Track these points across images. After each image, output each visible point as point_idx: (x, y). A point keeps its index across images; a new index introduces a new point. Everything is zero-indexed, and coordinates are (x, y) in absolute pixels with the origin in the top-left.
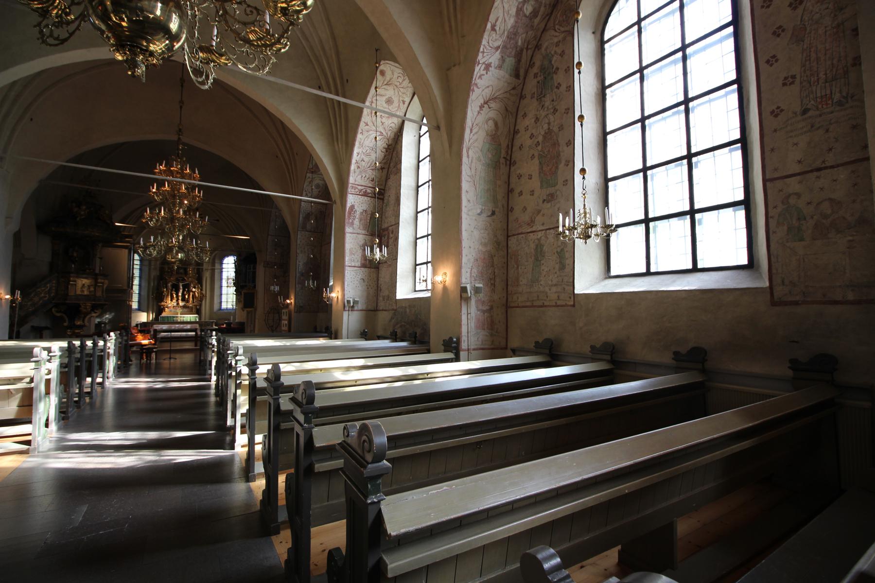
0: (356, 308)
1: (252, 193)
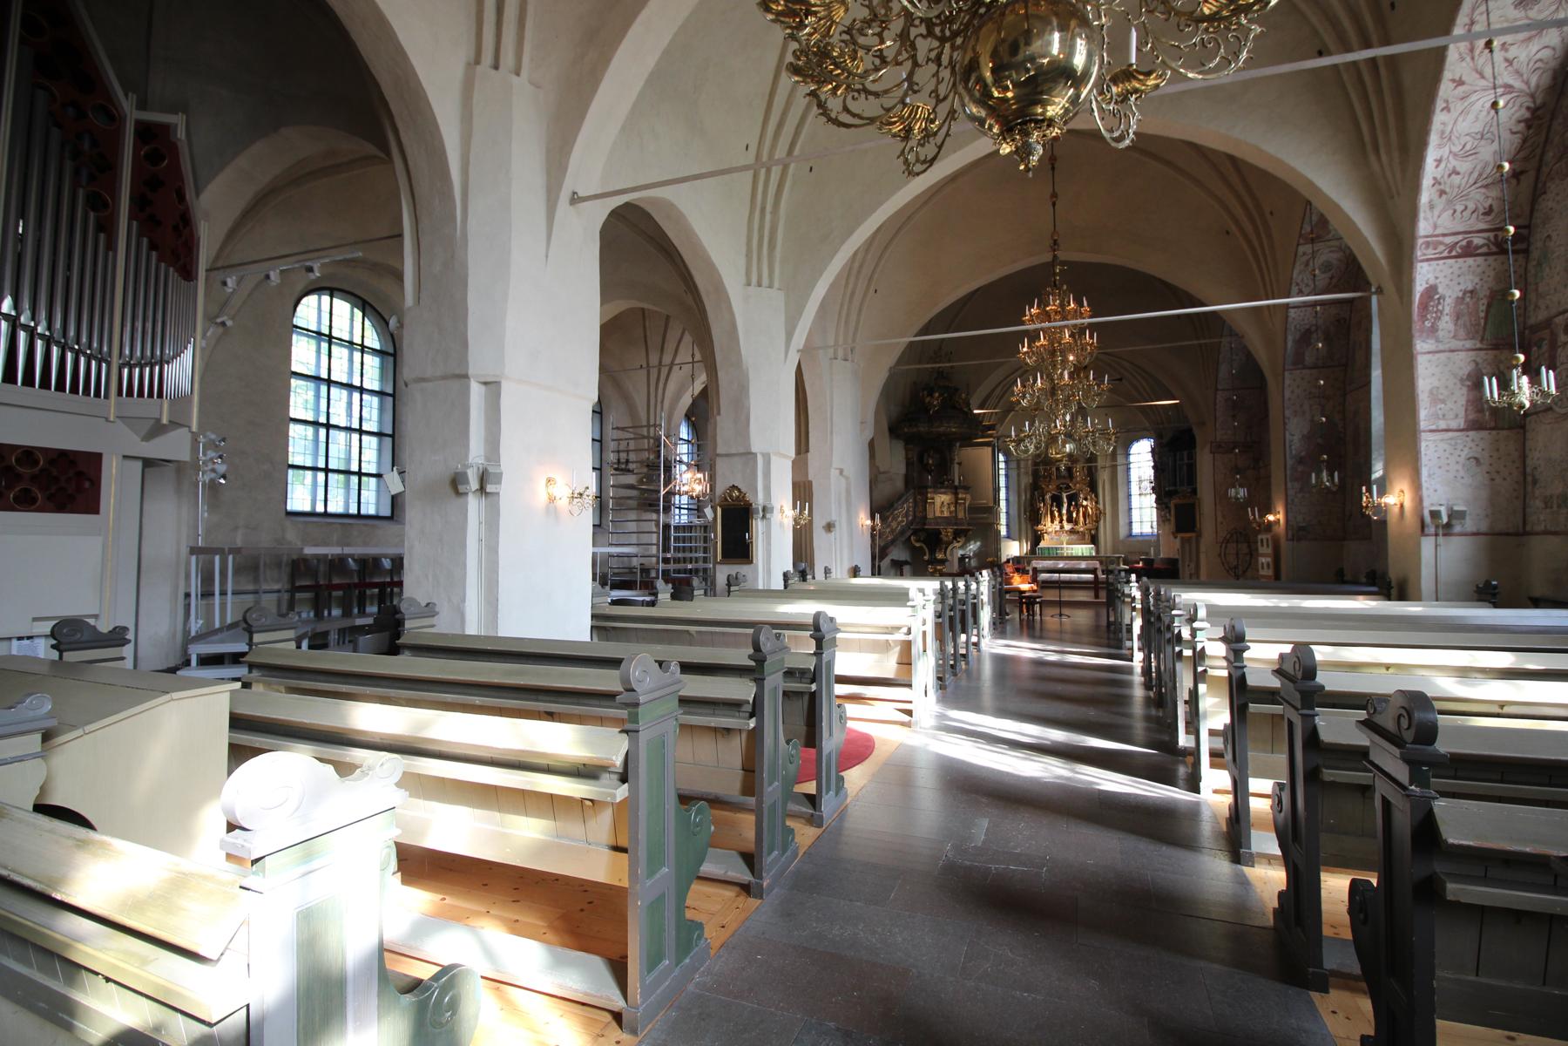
0: (1457, 529)
1: (1178, 316)
